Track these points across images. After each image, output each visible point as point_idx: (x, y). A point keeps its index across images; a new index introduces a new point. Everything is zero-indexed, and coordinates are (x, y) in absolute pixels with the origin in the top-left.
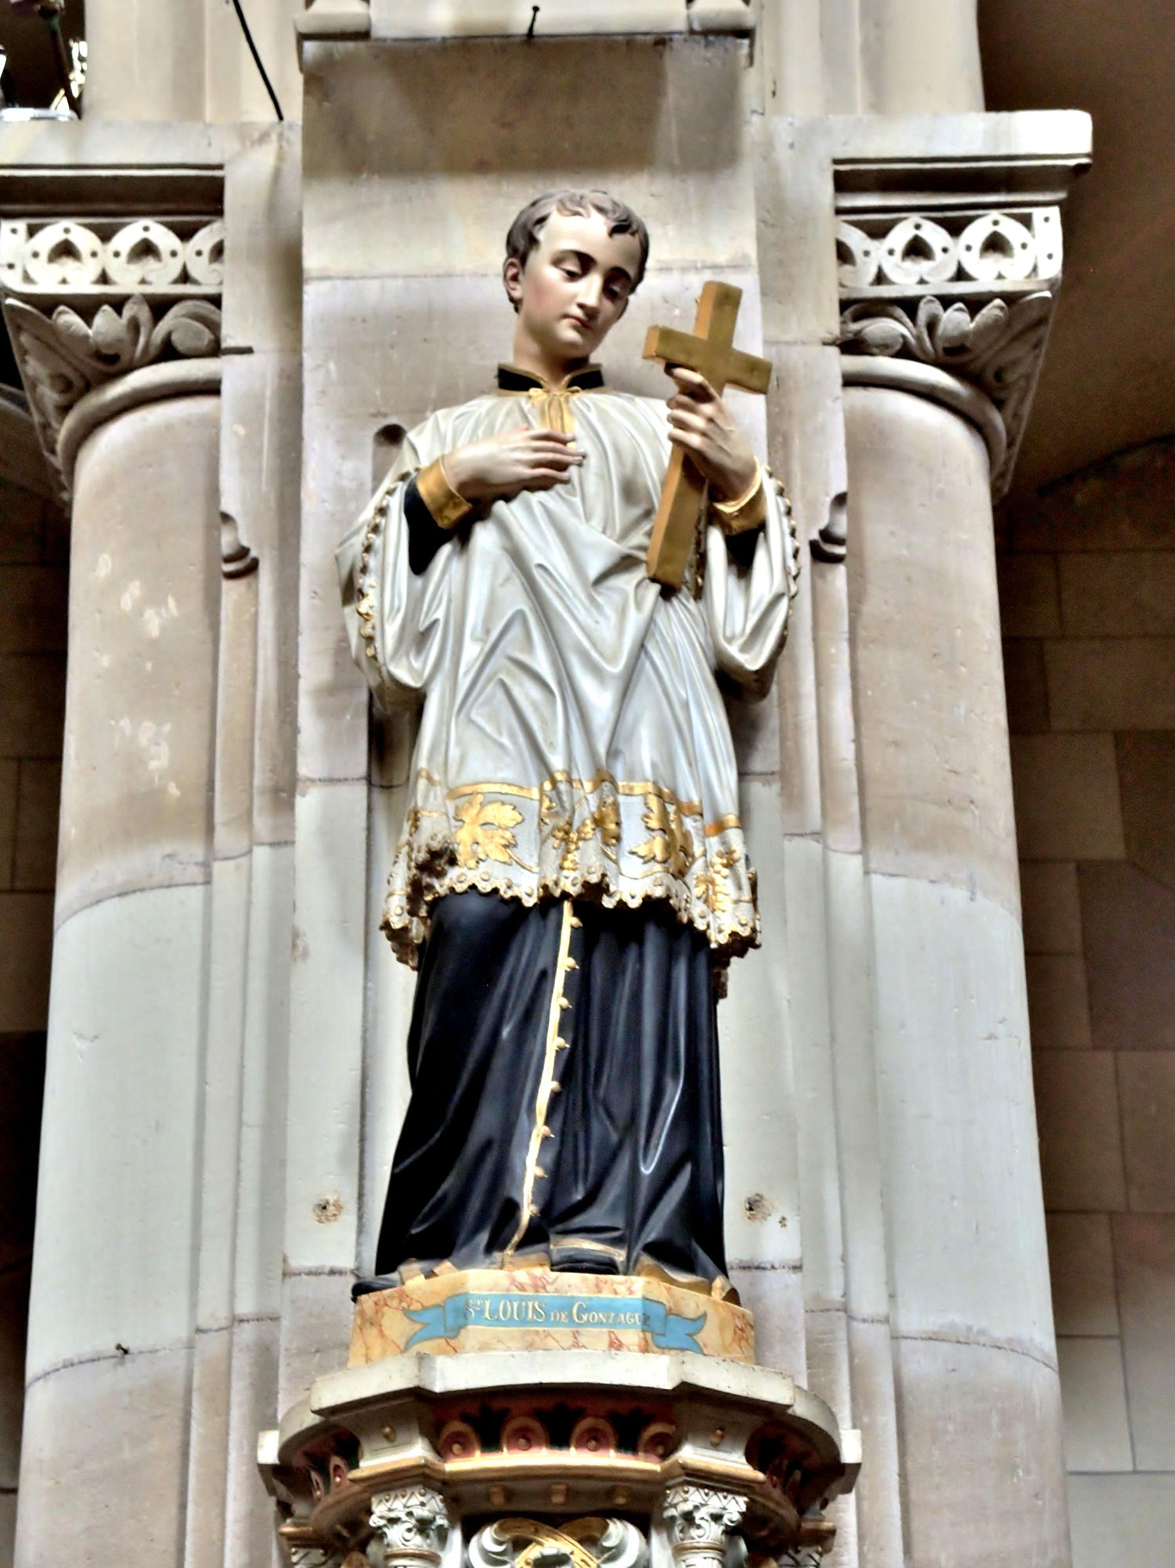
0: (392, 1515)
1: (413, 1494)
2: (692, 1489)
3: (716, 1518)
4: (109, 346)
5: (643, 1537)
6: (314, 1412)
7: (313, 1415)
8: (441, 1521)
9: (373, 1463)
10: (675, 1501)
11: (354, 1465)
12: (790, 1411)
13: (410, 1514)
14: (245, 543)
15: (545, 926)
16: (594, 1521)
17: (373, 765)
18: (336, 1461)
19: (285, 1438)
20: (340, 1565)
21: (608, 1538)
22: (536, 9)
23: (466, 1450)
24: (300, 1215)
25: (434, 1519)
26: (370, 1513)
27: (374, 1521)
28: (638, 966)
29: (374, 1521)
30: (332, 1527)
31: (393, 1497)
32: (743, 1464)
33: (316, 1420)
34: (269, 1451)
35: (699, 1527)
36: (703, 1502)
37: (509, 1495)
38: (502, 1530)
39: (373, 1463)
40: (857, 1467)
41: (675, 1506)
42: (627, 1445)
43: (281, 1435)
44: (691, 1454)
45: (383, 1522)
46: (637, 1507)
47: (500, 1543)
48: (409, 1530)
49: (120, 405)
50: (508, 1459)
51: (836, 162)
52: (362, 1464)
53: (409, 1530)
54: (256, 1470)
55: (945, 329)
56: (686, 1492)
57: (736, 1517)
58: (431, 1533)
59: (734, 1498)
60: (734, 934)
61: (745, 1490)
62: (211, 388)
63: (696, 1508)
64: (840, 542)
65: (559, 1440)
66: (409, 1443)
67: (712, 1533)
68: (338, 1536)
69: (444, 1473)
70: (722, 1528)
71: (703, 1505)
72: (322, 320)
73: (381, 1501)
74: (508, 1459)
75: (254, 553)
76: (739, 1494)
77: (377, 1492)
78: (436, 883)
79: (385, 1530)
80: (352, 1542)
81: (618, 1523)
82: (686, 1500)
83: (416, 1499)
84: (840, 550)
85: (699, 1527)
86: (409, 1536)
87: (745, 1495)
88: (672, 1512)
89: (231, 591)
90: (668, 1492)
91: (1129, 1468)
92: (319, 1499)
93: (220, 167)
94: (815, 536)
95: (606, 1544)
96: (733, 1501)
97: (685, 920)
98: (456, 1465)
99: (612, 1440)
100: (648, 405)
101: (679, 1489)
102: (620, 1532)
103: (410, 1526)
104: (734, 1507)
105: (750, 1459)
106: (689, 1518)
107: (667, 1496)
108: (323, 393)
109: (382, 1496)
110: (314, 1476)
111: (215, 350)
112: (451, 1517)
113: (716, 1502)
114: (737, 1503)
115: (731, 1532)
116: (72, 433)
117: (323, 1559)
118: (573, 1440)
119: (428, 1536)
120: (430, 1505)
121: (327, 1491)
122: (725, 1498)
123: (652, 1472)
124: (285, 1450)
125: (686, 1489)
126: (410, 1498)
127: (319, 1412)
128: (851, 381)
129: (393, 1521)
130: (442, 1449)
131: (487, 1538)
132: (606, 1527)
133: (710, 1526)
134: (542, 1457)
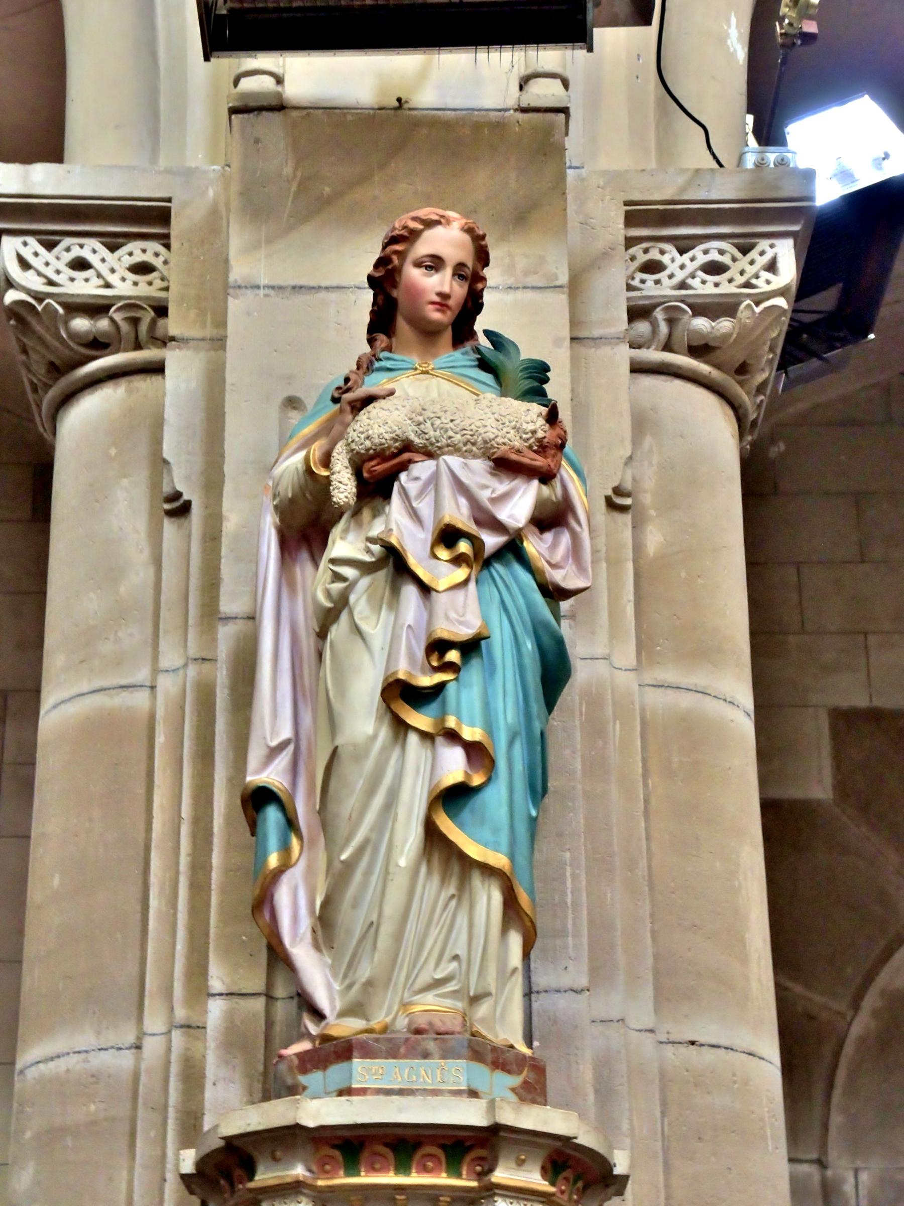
7: (219, 1140)
12: (575, 1141)
14: (179, 488)
24: (255, 755)
32: (540, 1180)
34: (188, 1161)
39: (265, 1176)
40: (624, 1179)
42: (454, 1169)
43: (197, 1152)
44: (501, 1175)
51: (626, 204)
52: (257, 1178)
54: (179, 1179)
64: (628, 495)
65: (403, 1167)
72: (109, 714)
75: (186, 497)
84: (628, 501)
89: (169, 527)
90: (483, 1201)
91: (562, 299)
93: (169, 200)
94: (609, 492)
98: (320, 1183)
108: (169, 610)
110: (222, 1182)
124: (201, 1164)
128: (638, 369)
134: (390, 1178)
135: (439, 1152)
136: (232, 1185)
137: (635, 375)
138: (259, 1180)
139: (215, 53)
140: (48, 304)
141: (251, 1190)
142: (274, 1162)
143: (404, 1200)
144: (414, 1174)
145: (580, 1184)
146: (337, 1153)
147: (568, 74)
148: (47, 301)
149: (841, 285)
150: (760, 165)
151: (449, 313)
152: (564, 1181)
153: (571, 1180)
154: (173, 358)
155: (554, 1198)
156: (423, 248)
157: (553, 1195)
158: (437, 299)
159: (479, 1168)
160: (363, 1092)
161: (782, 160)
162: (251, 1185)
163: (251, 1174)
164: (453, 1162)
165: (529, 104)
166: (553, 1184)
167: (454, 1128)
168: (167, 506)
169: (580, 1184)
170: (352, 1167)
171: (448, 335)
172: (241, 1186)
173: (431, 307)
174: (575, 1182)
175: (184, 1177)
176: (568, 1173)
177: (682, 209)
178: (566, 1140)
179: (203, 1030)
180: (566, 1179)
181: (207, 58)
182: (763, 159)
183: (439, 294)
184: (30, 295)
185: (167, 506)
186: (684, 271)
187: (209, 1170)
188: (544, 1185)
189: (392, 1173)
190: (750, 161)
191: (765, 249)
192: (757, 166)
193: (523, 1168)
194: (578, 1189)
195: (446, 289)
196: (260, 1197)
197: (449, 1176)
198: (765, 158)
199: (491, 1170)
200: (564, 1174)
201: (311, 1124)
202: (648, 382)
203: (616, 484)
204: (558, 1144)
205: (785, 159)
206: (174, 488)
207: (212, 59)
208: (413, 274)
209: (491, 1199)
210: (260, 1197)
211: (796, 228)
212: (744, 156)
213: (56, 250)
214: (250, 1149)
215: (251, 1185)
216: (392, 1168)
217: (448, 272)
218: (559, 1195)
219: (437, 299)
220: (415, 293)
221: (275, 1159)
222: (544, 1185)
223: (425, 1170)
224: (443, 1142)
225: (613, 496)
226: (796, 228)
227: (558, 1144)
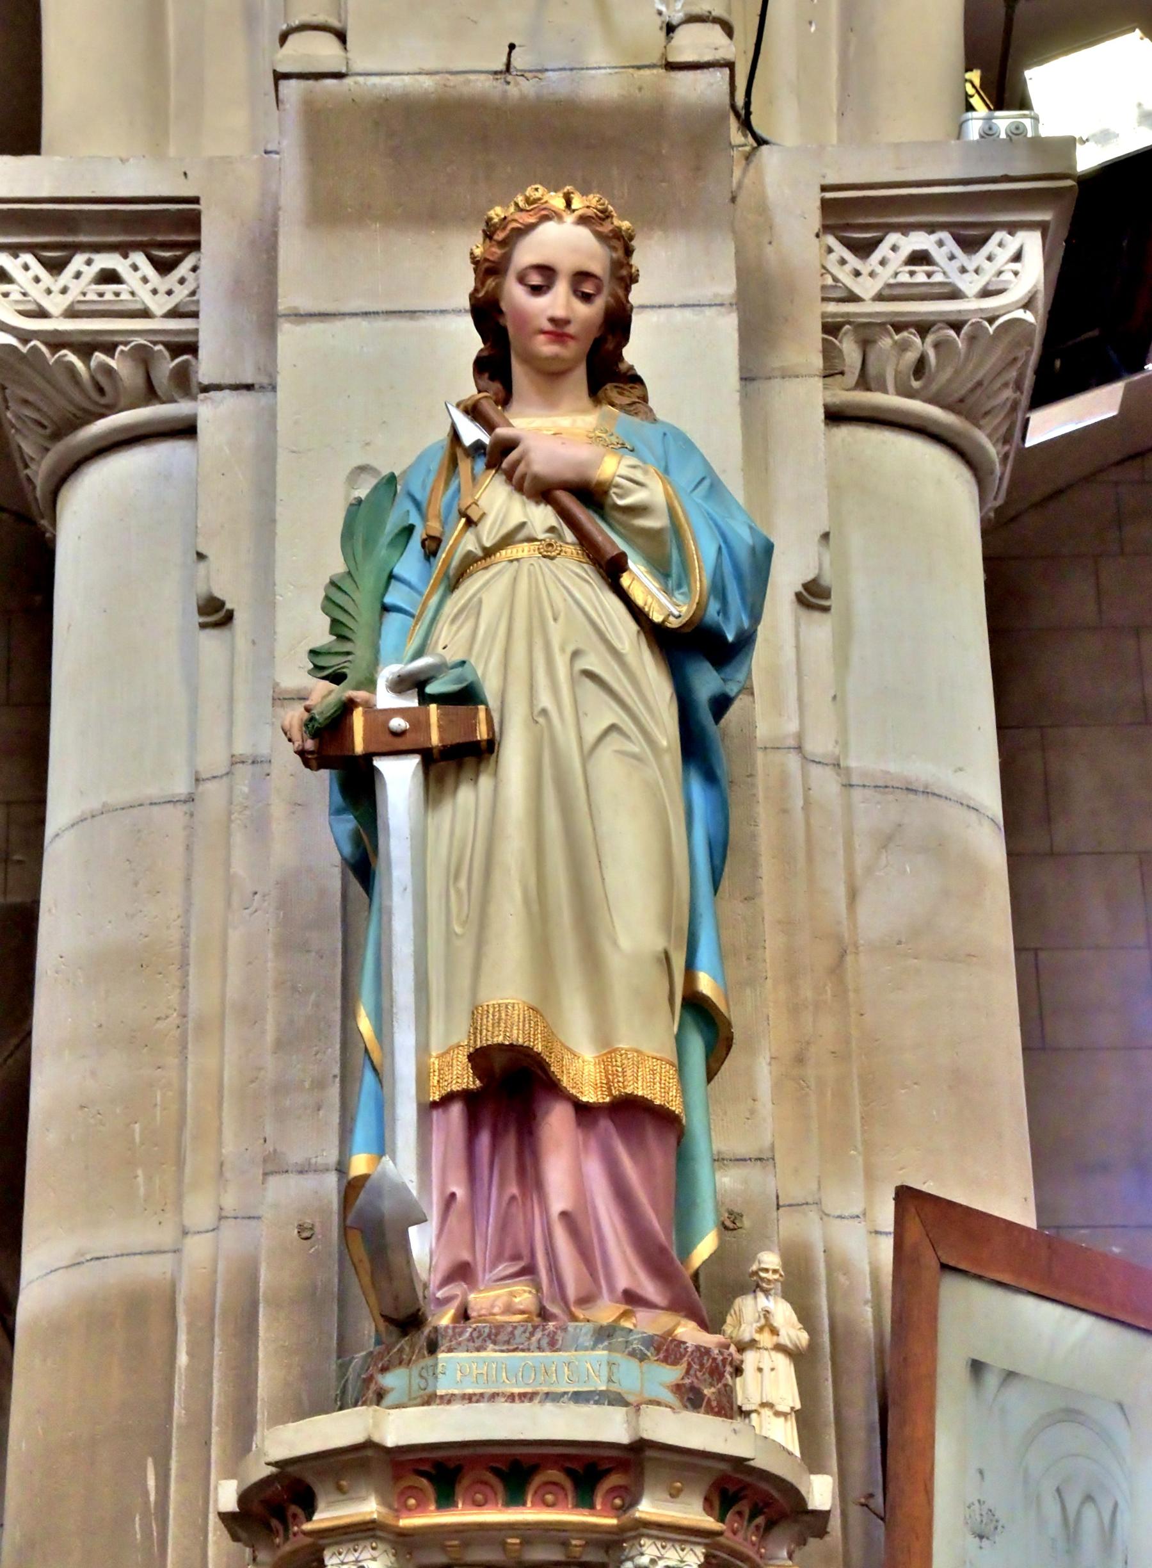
1: (365, 1547)
4: (326, 647)
6: (268, 1464)
9: (326, 1516)
10: (631, 1555)
11: (309, 1518)
12: (752, 1463)
15: (870, 1263)
18: (294, 1509)
22: (512, 47)
23: (421, 1507)
28: (348, 823)
33: (271, 1470)
34: (227, 1496)
36: (659, 1555)
39: (326, 1516)
42: (585, 1500)
44: (648, 1508)
50: (461, 1515)
51: (824, 189)
52: (316, 1517)
59: (692, 1550)
60: (126, 256)
62: (187, 430)
66: (364, 1499)
69: (397, 1527)
71: (660, 1558)
73: (349, 1550)
74: (461, 1515)
75: (228, 606)
82: (642, 1554)
89: (211, 642)
92: (278, 1546)
93: (196, 200)
98: (406, 1522)
109: (334, 1549)
111: (184, 383)
114: (695, 1554)
116: (52, 472)
121: (286, 1539)
122: (683, 1550)
124: (244, 1498)
126: (362, 1552)
127: (276, 1464)
128: (835, 416)
136: (286, 1530)
138: (322, 1520)
140: (34, 348)
142: (342, 1497)
143: (580, 1546)
145: (760, 1520)
146: (424, 1482)
148: (32, 343)
150: (988, 133)
151: (572, 344)
152: (737, 1518)
153: (747, 1516)
155: (722, 1539)
156: (526, 254)
157: (720, 1534)
158: (548, 326)
159: (618, 1502)
160: (448, 1399)
161: (1017, 128)
162: (308, 1527)
163: (310, 1510)
164: (584, 1495)
166: (721, 1519)
167: (524, 1445)
170: (446, 1500)
171: (579, 376)
172: (296, 1529)
173: (542, 338)
174: (752, 1517)
175: (225, 1517)
176: (745, 1507)
177: (49, 211)
178: (739, 1463)
180: (740, 1514)
182: (990, 129)
183: (552, 320)
184: (16, 336)
186: (66, 296)
187: (256, 1507)
188: (709, 1522)
190: (974, 128)
191: (1002, 246)
192: (981, 137)
193: (678, 1500)
194: (757, 1527)
195: (560, 313)
196: (322, 1542)
198: (994, 127)
199: (635, 1502)
200: (735, 1508)
201: (390, 1441)
202: (845, 433)
204: (722, 1466)
205: (1021, 126)
206: (209, 587)
208: (515, 294)
209: (636, 1542)
210: (322, 1542)
211: (1046, 216)
212: (965, 125)
213: (876, 256)
214: (310, 1479)
215: (308, 1527)
217: (561, 288)
218: (728, 1534)
219: (548, 326)
220: (523, 318)
221: (340, 1490)
222: (709, 1522)
224: (568, 1465)
226: (1046, 216)
227: (722, 1466)
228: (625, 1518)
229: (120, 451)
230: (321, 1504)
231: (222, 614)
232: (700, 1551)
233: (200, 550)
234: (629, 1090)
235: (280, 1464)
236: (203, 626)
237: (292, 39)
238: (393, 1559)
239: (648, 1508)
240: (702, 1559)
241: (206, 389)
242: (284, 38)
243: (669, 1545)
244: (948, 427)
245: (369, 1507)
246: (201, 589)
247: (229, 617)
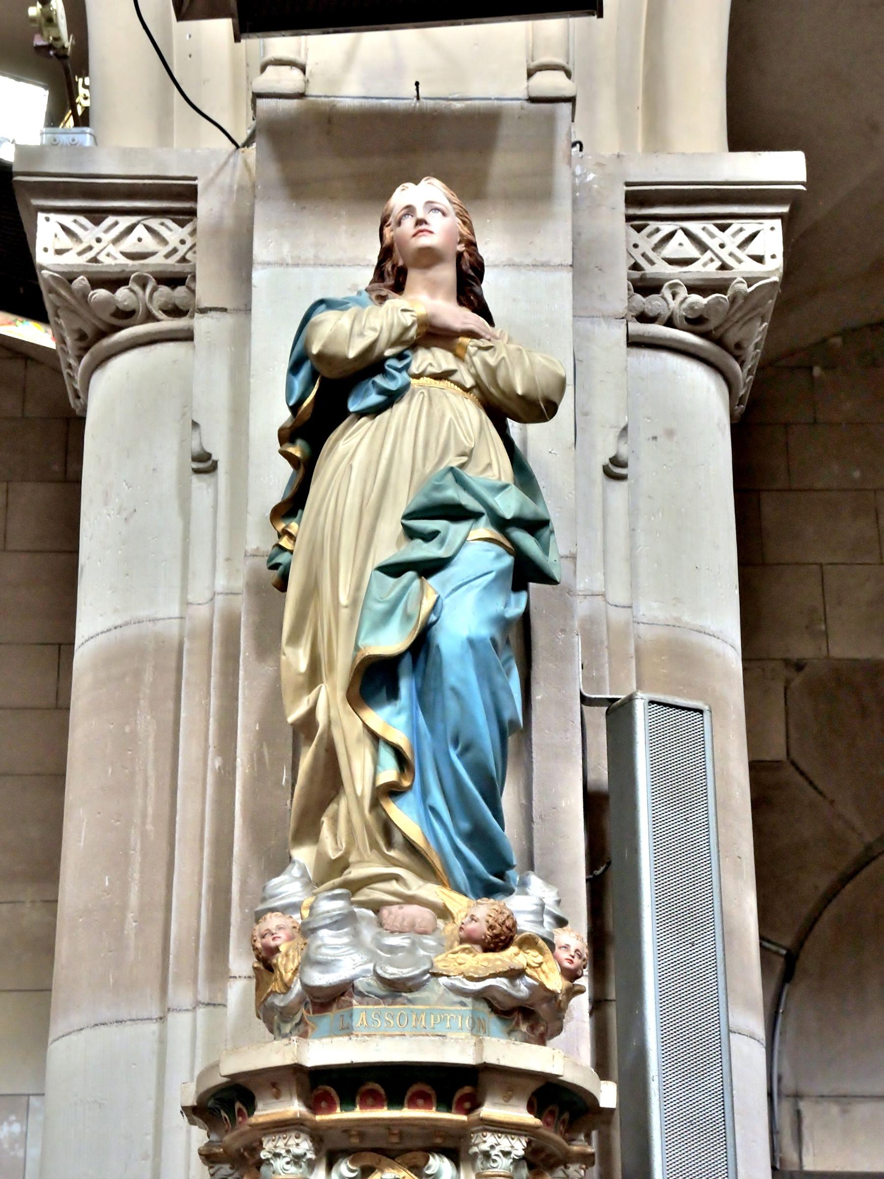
0: (278, 1151)
2: (489, 1134)
3: (506, 1154)
5: (455, 1168)
8: (311, 1155)
10: (476, 1142)
12: (561, 1078)
13: (288, 1151)
16: (420, 1155)
17: (385, 816)
18: (238, 1105)
19: (203, 1089)
20: (242, 1177)
21: (428, 1168)
23: (331, 1109)
25: (305, 1154)
26: (261, 1146)
27: (264, 1155)
29: (264, 1155)
30: (238, 1150)
31: (277, 1137)
35: (494, 1161)
37: (361, 1135)
38: (353, 1162)
41: (477, 1145)
42: (445, 1104)
45: (270, 1156)
46: (450, 1144)
47: (352, 1171)
48: (288, 1163)
49: (127, 344)
51: (628, 184)
53: (288, 1163)
55: (620, 327)
56: (485, 1137)
57: (521, 1153)
58: (303, 1164)
61: (526, 1133)
62: (187, 336)
63: (492, 1147)
65: (396, 1102)
67: (503, 1165)
68: (242, 1156)
69: (315, 1121)
70: (511, 1161)
75: (214, 458)
76: (520, 1135)
77: (265, 1135)
78: (482, 1034)
79: (272, 1161)
80: (251, 1161)
81: (436, 1156)
82: (485, 1142)
83: (292, 1141)
85: (494, 1161)
86: (288, 1167)
87: (525, 1136)
88: (475, 1149)
89: (199, 484)
91: (566, 278)
93: (195, 179)
94: (607, 461)
95: (428, 1172)
96: (518, 1142)
97: (246, 682)
99: (434, 1100)
100: (574, 69)
101: (480, 1134)
102: (439, 1164)
103: (288, 1159)
104: (518, 1147)
105: (531, 1109)
106: (487, 1155)
107: (471, 1138)
112: (317, 1152)
113: (505, 1143)
115: (516, 1162)
117: (231, 1171)
118: (406, 1101)
119: (301, 1167)
120: (303, 1146)
123: (463, 1122)
125: (485, 1134)
128: (635, 343)
129: (277, 1155)
130: (314, 1106)
131: (344, 1168)
132: (428, 1159)
133: (502, 1161)
134: (384, 1113)
135: (427, 1089)
136: (233, 1120)
137: (635, 351)
139: (245, 35)
141: (254, 1126)
144: (358, 1108)
145: (566, 1116)
147: (570, 67)
149: (508, 420)
153: (557, 1115)
154: (201, 324)
157: (538, 1127)
163: (251, 1106)
165: (255, 287)
168: (195, 465)
169: (566, 1116)
174: (561, 1113)
179: (47, 993)
181: (237, 39)
185: (195, 465)
189: (386, 1108)
197: (438, 1110)
200: (551, 1108)
202: (648, 357)
203: (612, 454)
207: (243, 41)
215: (253, 1120)
216: (386, 1103)
222: (530, 1119)
223: (364, 1106)
225: (611, 466)
228: (474, 1116)
229: (650, 1116)
230: (260, 1105)
231: (210, 463)
232: (524, 1141)
233: (195, 420)
234: (367, 654)
235: (232, 1077)
236: (197, 471)
237: (270, 69)
238: (311, 1144)
239: (490, 1110)
240: (525, 1145)
241: (203, 311)
242: (263, 69)
243: (503, 1136)
244: (694, 345)
245: (294, 1108)
246: (195, 447)
247: (214, 467)
